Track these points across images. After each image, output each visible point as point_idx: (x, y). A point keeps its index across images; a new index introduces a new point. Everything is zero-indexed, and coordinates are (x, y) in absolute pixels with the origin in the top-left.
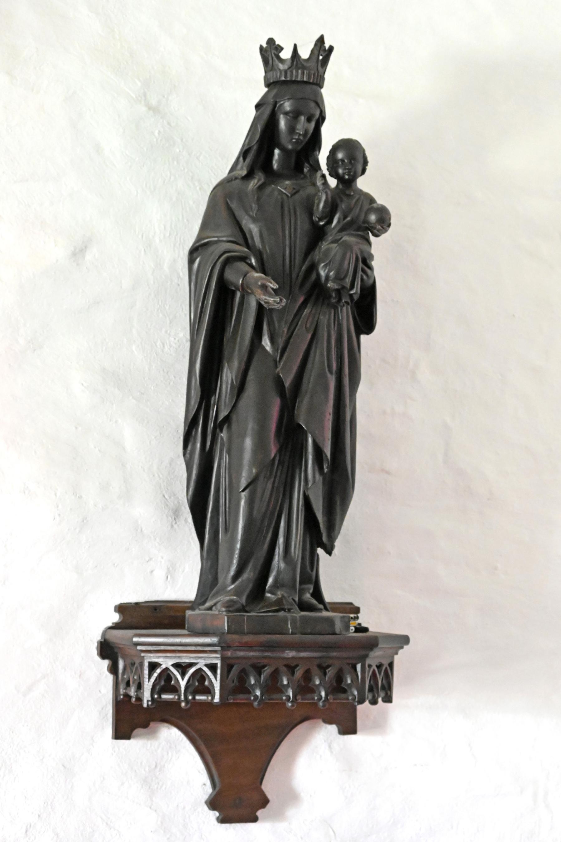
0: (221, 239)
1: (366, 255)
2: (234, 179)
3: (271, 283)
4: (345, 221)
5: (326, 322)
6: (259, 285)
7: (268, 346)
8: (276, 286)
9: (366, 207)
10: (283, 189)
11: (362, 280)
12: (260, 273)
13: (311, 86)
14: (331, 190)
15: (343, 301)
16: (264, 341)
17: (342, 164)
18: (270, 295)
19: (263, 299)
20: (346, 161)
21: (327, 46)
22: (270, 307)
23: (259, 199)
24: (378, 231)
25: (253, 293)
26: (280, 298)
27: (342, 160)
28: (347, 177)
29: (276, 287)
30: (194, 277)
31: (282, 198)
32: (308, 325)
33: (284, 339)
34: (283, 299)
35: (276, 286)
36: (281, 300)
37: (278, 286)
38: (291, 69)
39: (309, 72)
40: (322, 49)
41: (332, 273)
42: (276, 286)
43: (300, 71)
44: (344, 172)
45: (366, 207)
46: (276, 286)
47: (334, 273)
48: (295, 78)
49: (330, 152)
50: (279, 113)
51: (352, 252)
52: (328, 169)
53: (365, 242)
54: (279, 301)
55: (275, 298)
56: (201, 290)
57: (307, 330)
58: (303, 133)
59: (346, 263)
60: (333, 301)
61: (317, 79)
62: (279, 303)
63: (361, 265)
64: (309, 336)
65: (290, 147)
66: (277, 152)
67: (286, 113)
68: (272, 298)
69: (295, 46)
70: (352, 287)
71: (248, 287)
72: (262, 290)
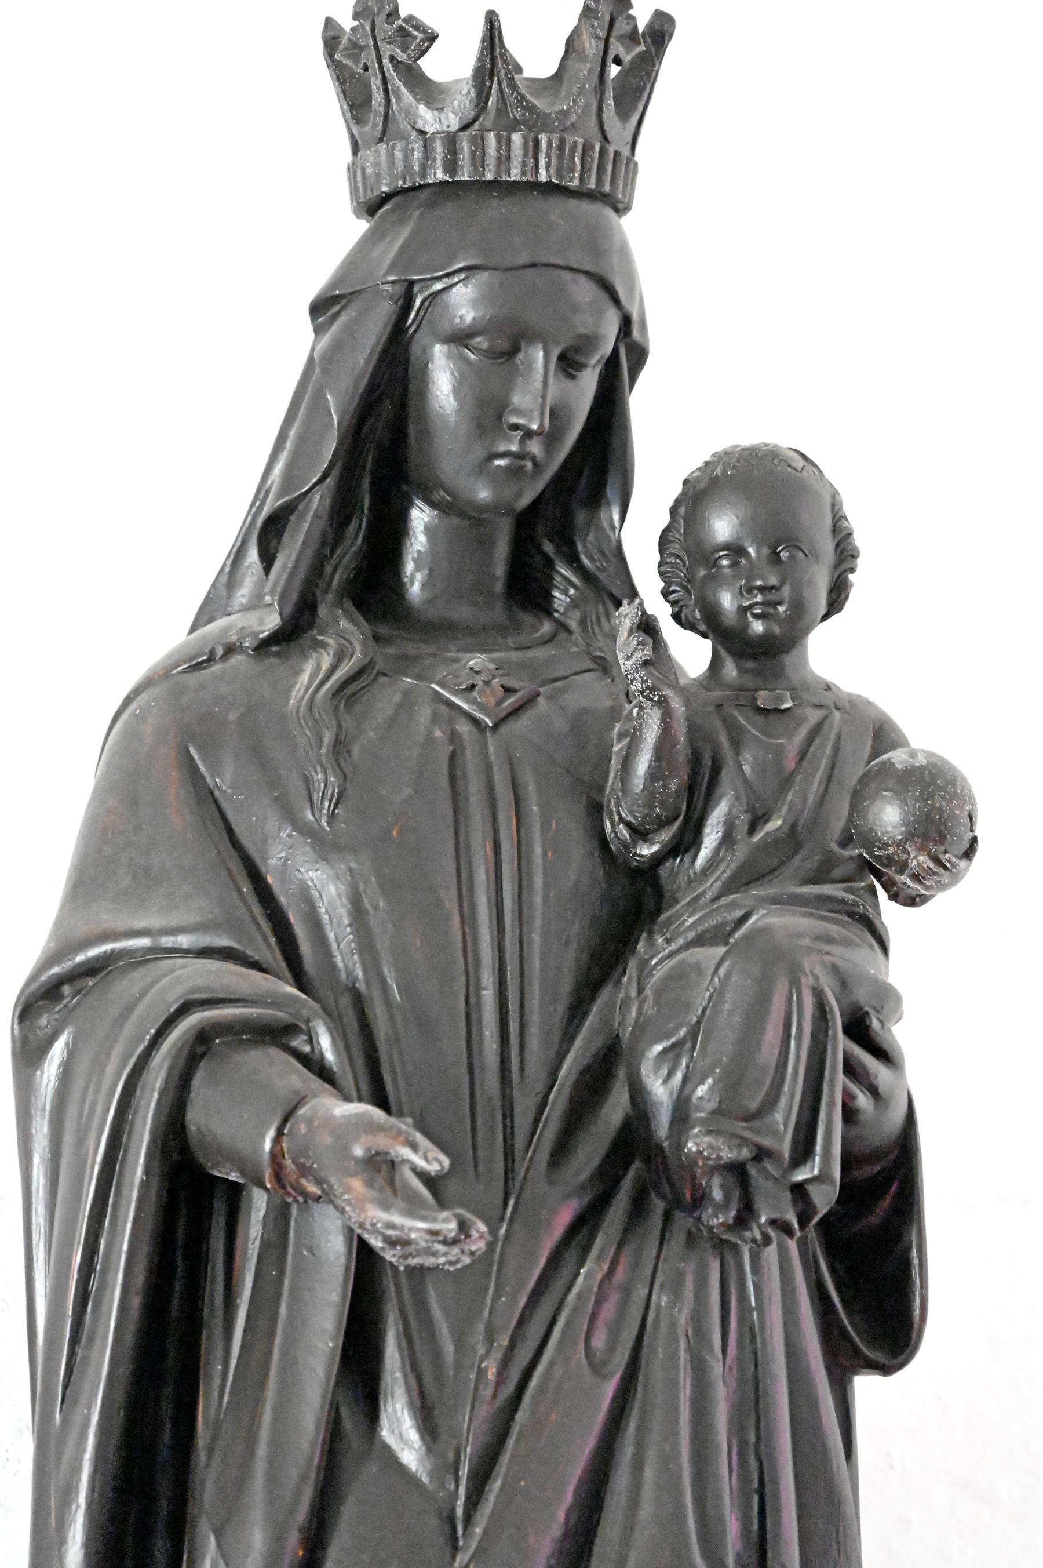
0: (167, 941)
1: (862, 996)
2: (220, 652)
3: (414, 1147)
4: (758, 837)
5: (683, 1317)
6: (357, 1161)
7: (412, 1448)
8: (436, 1162)
9: (852, 773)
10: (455, 693)
11: (850, 1114)
12: (368, 1102)
13: (573, 203)
14: (685, 692)
15: (763, 1220)
16: (391, 1423)
17: (734, 565)
18: (413, 1207)
19: (379, 1225)
20: (752, 551)
21: (642, 13)
22: (413, 1262)
23: (340, 747)
24: (916, 877)
25: (326, 1197)
26: (457, 1216)
27: (736, 550)
28: (758, 627)
29: (440, 1163)
30: (41, 1128)
31: (453, 736)
32: (599, 1341)
33: (485, 1411)
34: (475, 1223)
35: (436, 1162)
36: (464, 1226)
37: (446, 1162)
38: (473, 130)
39: (562, 142)
40: (622, 27)
41: (702, 1090)
42: (437, 1159)
43: (517, 138)
44: (746, 604)
45: (852, 773)
46: (437, 1159)
47: (711, 1088)
48: (498, 173)
49: (674, 511)
50: (422, 339)
51: (795, 982)
52: (665, 594)
53: (858, 933)
54: (453, 1234)
55: (434, 1220)
56: (77, 1196)
57: (598, 1369)
58: (541, 425)
59: (771, 1036)
60: (716, 1219)
61: (601, 169)
62: (455, 1242)
63: (841, 1043)
64: (609, 1389)
65: (484, 494)
66: (420, 516)
67: (460, 338)
68: (423, 1219)
69: (492, 23)
70: (803, 1151)
71: (304, 1171)
72: (369, 1183)
